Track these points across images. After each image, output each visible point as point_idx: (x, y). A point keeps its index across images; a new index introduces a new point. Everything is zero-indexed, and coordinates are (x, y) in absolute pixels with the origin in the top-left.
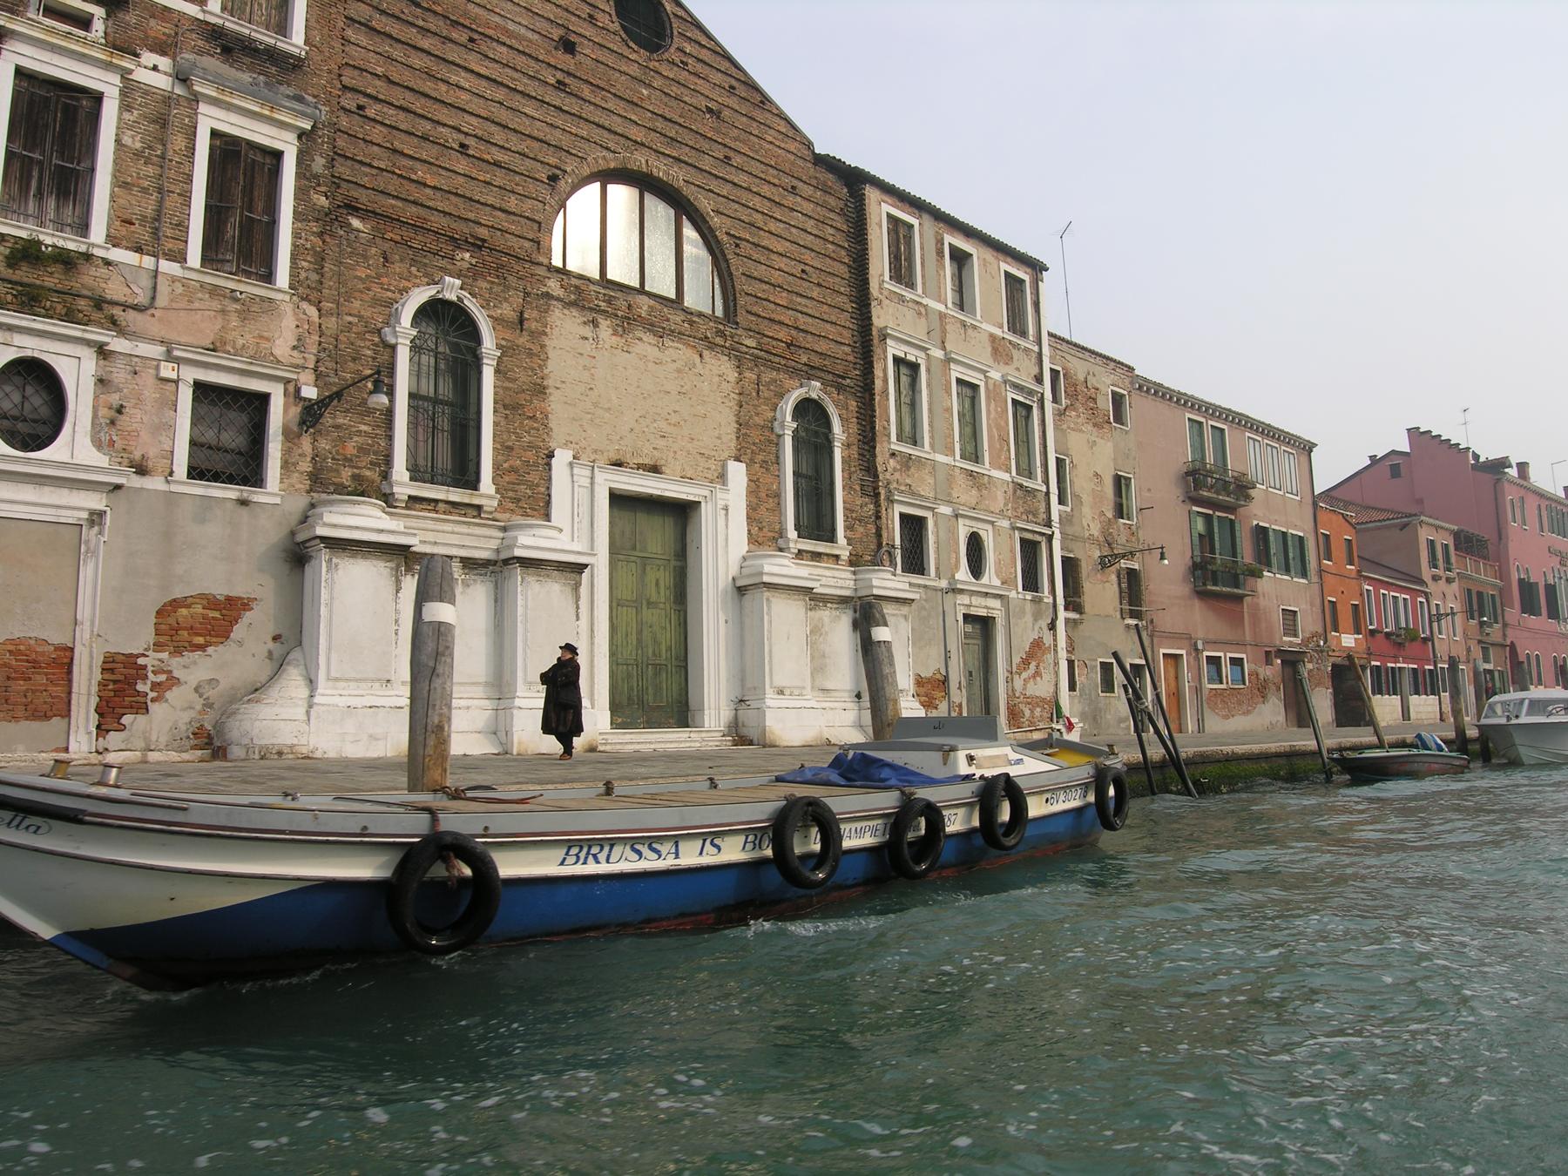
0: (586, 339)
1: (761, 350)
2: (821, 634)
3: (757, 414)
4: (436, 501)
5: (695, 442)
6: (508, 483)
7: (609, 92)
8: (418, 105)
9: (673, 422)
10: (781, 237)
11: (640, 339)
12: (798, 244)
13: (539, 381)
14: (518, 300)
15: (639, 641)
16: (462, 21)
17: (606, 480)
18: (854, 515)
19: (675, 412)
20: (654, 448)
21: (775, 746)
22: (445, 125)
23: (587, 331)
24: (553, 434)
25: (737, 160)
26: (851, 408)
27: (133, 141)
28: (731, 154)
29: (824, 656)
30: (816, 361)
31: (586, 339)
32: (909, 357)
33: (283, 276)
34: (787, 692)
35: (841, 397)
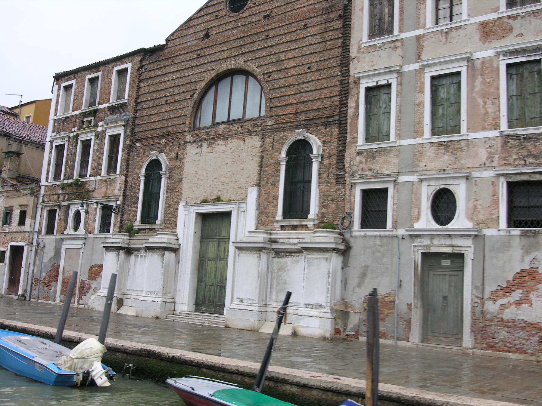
0: (197, 153)
1: (278, 124)
2: (285, 271)
3: (272, 158)
4: (145, 229)
5: (237, 183)
6: (169, 218)
7: (216, 45)
8: (155, 95)
9: (228, 176)
10: (295, 57)
11: (218, 145)
12: (306, 55)
13: (181, 177)
14: (176, 148)
15: (215, 275)
16: (170, 57)
17: (194, 210)
18: (329, 198)
19: (229, 171)
20: (219, 191)
21: (229, 327)
22: (162, 97)
23: (198, 150)
24: (183, 196)
25: (272, 33)
26: (334, 133)
27: (96, 148)
28: (199, 52)
29: (285, 283)
30: (311, 115)
31: (197, 153)
32: (380, 83)
33: (118, 172)
34: (245, 301)
35: (328, 129)
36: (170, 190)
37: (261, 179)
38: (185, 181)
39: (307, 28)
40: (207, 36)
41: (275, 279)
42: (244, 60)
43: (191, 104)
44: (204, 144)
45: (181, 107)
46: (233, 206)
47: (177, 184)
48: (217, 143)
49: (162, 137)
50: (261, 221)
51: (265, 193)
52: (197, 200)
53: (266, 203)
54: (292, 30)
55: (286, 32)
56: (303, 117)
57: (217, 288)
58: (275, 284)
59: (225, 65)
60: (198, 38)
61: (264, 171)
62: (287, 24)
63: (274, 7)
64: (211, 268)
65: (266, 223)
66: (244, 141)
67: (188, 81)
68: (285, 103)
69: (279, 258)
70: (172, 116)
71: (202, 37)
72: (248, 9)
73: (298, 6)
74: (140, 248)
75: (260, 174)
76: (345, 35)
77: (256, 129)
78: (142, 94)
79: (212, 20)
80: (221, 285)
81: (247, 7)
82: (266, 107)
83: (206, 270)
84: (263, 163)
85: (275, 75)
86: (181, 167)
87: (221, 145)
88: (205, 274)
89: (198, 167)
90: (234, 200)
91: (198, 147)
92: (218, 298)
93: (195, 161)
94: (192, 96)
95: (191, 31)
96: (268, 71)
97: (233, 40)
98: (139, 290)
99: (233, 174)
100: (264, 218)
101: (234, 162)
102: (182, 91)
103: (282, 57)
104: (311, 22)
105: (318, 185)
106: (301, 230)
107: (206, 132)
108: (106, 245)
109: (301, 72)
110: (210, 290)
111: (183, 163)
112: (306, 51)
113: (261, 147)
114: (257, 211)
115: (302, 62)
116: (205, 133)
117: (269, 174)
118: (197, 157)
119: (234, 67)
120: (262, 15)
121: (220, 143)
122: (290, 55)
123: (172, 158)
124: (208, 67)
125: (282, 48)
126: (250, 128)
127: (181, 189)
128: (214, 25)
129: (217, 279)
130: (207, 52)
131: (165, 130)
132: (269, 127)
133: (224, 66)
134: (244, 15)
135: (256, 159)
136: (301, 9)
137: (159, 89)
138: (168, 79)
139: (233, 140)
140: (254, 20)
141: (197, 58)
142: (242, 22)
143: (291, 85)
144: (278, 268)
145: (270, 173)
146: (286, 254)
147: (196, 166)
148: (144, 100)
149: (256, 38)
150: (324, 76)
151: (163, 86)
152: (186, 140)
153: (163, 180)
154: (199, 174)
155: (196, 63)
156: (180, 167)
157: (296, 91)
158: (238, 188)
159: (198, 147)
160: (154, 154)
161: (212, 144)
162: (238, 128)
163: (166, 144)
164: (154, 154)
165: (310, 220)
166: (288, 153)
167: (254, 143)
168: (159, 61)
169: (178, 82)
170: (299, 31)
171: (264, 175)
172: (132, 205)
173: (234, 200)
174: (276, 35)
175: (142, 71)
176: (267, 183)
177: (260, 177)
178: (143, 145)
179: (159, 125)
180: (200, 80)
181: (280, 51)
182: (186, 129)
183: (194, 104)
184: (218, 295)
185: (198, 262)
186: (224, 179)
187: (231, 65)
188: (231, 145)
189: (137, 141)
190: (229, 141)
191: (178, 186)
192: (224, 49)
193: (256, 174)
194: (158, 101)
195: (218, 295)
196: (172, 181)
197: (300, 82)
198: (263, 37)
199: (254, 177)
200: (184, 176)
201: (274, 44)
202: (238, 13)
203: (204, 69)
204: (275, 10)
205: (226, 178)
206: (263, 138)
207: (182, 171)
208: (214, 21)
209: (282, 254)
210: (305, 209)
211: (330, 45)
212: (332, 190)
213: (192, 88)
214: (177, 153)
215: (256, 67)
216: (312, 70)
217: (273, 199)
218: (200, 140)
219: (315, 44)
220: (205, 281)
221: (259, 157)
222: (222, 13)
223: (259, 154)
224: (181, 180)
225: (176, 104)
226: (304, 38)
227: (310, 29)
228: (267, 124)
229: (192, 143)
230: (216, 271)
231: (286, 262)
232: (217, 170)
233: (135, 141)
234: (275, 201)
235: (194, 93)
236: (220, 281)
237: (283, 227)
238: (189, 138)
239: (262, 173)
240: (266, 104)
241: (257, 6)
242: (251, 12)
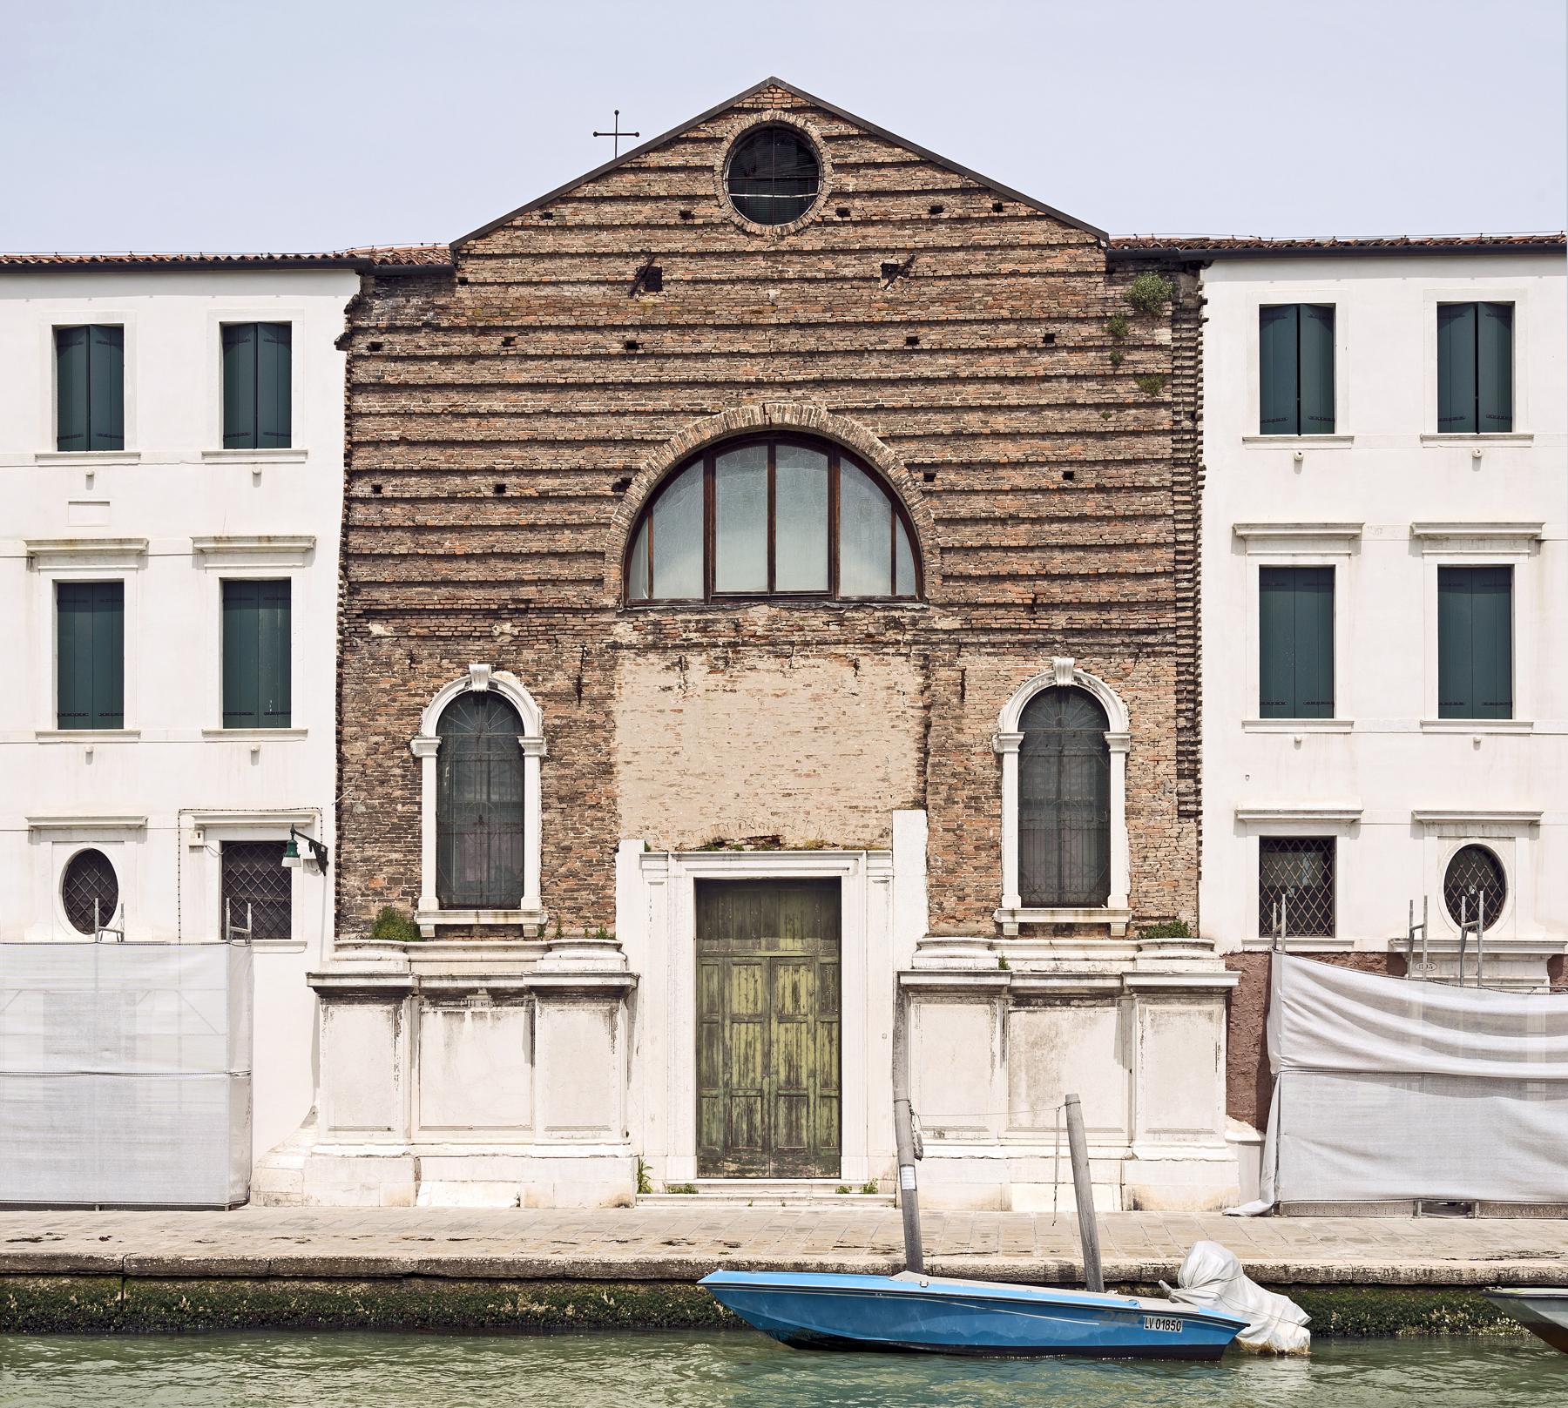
0: (670, 688)
3: (960, 730)
11: (752, 669)
13: (604, 759)
19: (808, 757)
23: (673, 678)
25: (930, 337)
31: (670, 688)
36: (561, 799)
37: (929, 789)
39: (1056, 348)
40: (650, 279)
42: (832, 406)
43: (620, 516)
44: (696, 660)
45: (575, 519)
46: (850, 863)
47: (590, 782)
48: (748, 662)
50: (941, 908)
51: (945, 830)
52: (685, 839)
53: (953, 858)
54: (1002, 344)
55: (983, 344)
57: (776, 1104)
60: (611, 278)
61: (933, 765)
62: (983, 321)
63: (921, 245)
64: (748, 1044)
65: (959, 915)
66: (856, 667)
68: (994, 570)
72: (818, 224)
73: (1009, 267)
74: (474, 991)
75: (925, 773)
77: (891, 635)
78: (368, 443)
79: (667, 226)
80: (793, 1092)
81: (812, 215)
83: (727, 1053)
84: (930, 741)
85: (945, 478)
86: (603, 726)
87: (768, 671)
88: (725, 1064)
90: (834, 845)
91: (668, 668)
92: (783, 1131)
93: (661, 711)
94: (624, 485)
96: (927, 461)
97: (778, 326)
98: (480, 1128)
99: (825, 766)
100: (950, 902)
101: (824, 728)
103: (973, 421)
104: (1069, 333)
107: (698, 622)
109: (1044, 483)
110: (750, 1111)
111: (608, 714)
113: (922, 693)
115: (1047, 453)
117: (954, 775)
118: (671, 700)
119: (794, 422)
120: (878, 261)
121: (760, 665)
122: (1000, 422)
123: (556, 694)
125: (971, 394)
126: (872, 630)
128: (678, 246)
129: (774, 1077)
130: (670, 342)
131: (505, 594)
133: (751, 412)
135: (908, 726)
136: (1022, 280)
137: (460, 437)
138: (499, 406)
139: (812, 661)
140: (847, 272)
141: (622, 357)
142: (798, 267)
143: (1011, 517)
144: (1031, 1039)
145: (960, 773)
148: (384, 466)
149: (868, 338)
151: (473, 430)
152: (612, 639)
153: (532, 767)
154: (684, 756)
155: (619, 372)
157: (1030, 540)
158: (847, 811)
159: (668, 668)
160: (480, 677)
161: (727, 664)
163: (519, 642)
164: (479, 674)
165: (1115, 913)
166: (1024, 719)
167: (895, 677)
168: (438, 328)
170: (1024, 353)
171: (938, 775)
172: (377, 841)
173: (834, 845)
174: (946, 346)
176: (950, 801)
177: (926, 782)
178: (402, 634)
180: (649, 437)
181: (964, 403)
182: (610, 601)
184: (781, 1121)
186: (791, 782)
187: (785, 411)
188: (804, 675)
190: (797, 661)
192: (744, 348)
193: (913, 772)
195: (781, 1121)
196: (563, 772)
197: (1044, 514)
198: (896, 339)
201: (943, 374)
202: (778, 228)
203: (666, 404)
204: (924, 259)
205: (800, 775)
206: (926, 667)
207: (606, 740)
208: (678, 234)
209: (1040, 1001)
211: (1136, 419)
212: (1169, 832)
213: (617, 462)
214: (579, 679)
216: (1081, 486)
218: (675, 647)
219: (1084, 406)
220: (726, 1084)
222: (702, 211)
224: (606, 770)
226: (1047, 378)
228: (936, 627)
230: (767, 1055)
236: (788, 1081)
239: (929, 770)
241: (855, 224)
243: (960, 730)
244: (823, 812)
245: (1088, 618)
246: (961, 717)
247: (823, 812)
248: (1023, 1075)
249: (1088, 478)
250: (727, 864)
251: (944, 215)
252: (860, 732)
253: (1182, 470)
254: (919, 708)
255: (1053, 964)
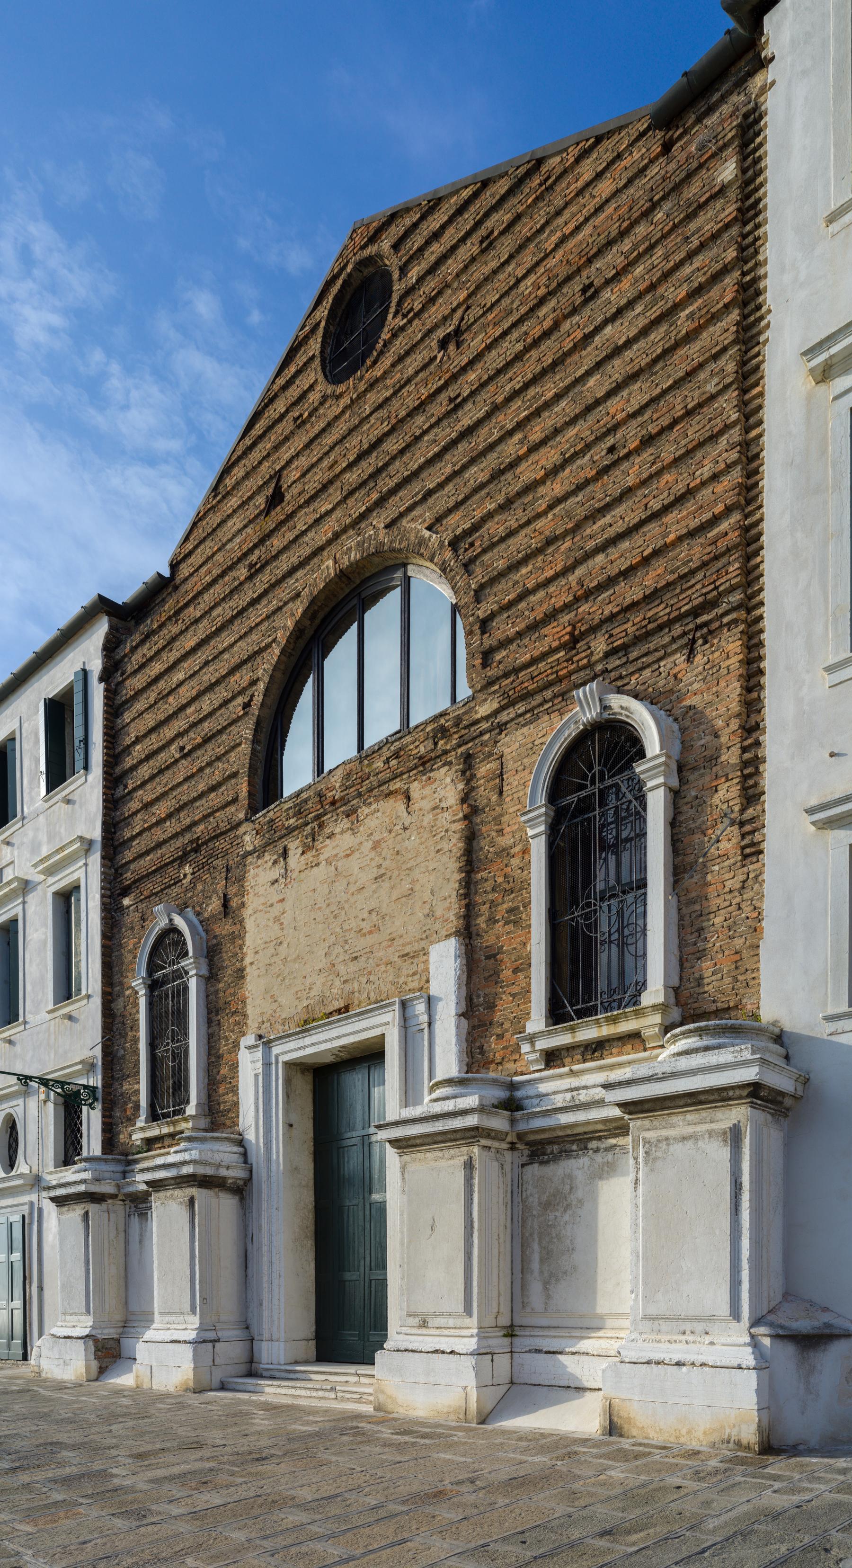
0: (276, 881)
2: (568, 1207)
38: (251, 973)
41: (536, 1236)
49: (182, 859)
56: (599, 645)
58: (536, 1257)
59: (330, 562)
66: (409, 798)
67: (235, 660)
69: (542, 1163)
70: (201, 787)
71: (262, 507)
76: (748, 828)
82: (471, 655)
87: (342, 833)
89: (282, 924)
93: (271, 905)
95: (234, 502)
101: (382, 876)
102: (221, 701)
105: (672, 880)
106: (620, 1054)
108: (53, 1194)
111: (241, 922)
112: (596, 385)
114: (464, 1022)
116: (291, 813)
124: (282, 593)
127: (244, 1002)
131: (188, 837)
132: (485, 725)
134: (378, 372)
139: (374, 806)
144: (544, 1198)
146: (568, 1146)
147: (276, 919)
150: (667, 456)
156: (234, 938)
162: (387, 761)
169: (208, 676)
175: (116, 681)
176: (492, 920)
179: (171, 827)
183: (256, 730)
185: (311, 1216)
186: (361, 944)
188: (372, 823)
189: (125, 892)
191: (234, 994)
194: (163, 755)
199: (449, 909)
200: (248, 960)
205: (364, 935)
207: (241, 948)
209: (556, 1148)
210: (630, 979)
213: (245, 682)
215: (429, 528)
217: (516, 971)
221: (457, 836)
223: (459, 826)
225: (209, 746)
227: (606, 294)
228: (479, 716)
229: (260, 852)
231: (570, 1176)
232: (335, 917)
233: (119, 895)
234: (521, 975)
235: (253, 696)
237: (552, 1058)
238: (249, 840)
240: (468, 645)
242: (400, 345)
243: (501, 832)
244: (383, 968)
245: (630, 627)
246: (502, 815)
247: (383, 968)
248: (536, 1247)
249: (631, 435)
250: (301, 1043)
251: (496, 233)
252: (409, 869)
253: (730, 218)
254: (459, 820)
255: (568, 1096)
